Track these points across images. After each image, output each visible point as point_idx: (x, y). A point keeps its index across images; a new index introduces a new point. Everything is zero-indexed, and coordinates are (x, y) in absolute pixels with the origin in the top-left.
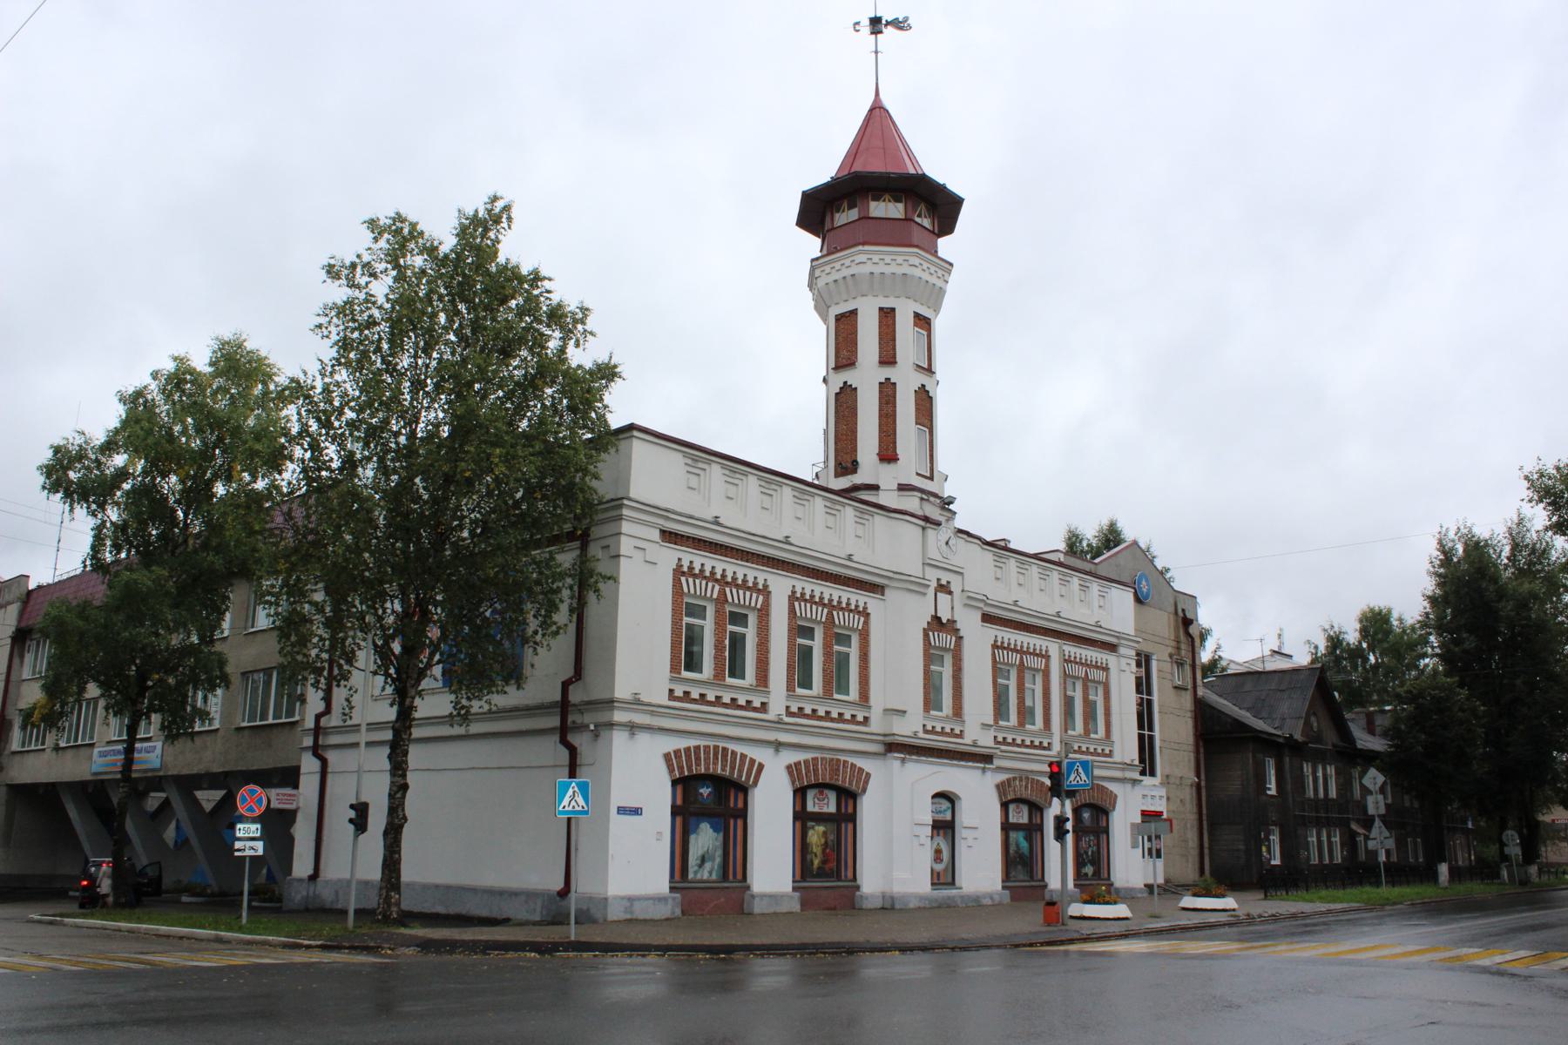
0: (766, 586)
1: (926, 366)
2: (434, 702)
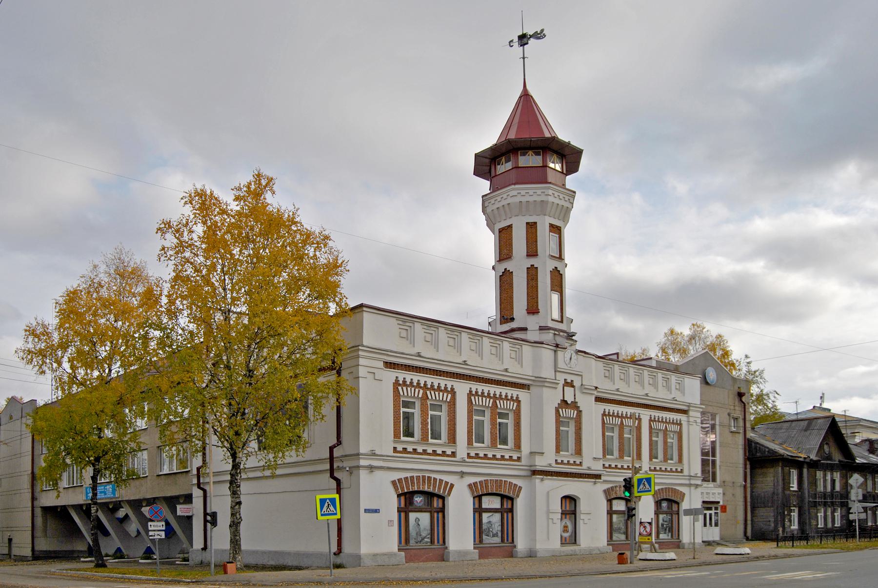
0: (517, 398)
1: (558, 256)
2: (253, 459)
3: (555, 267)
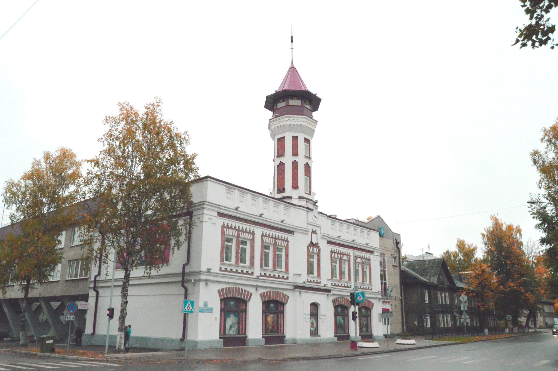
0: (253, 232)
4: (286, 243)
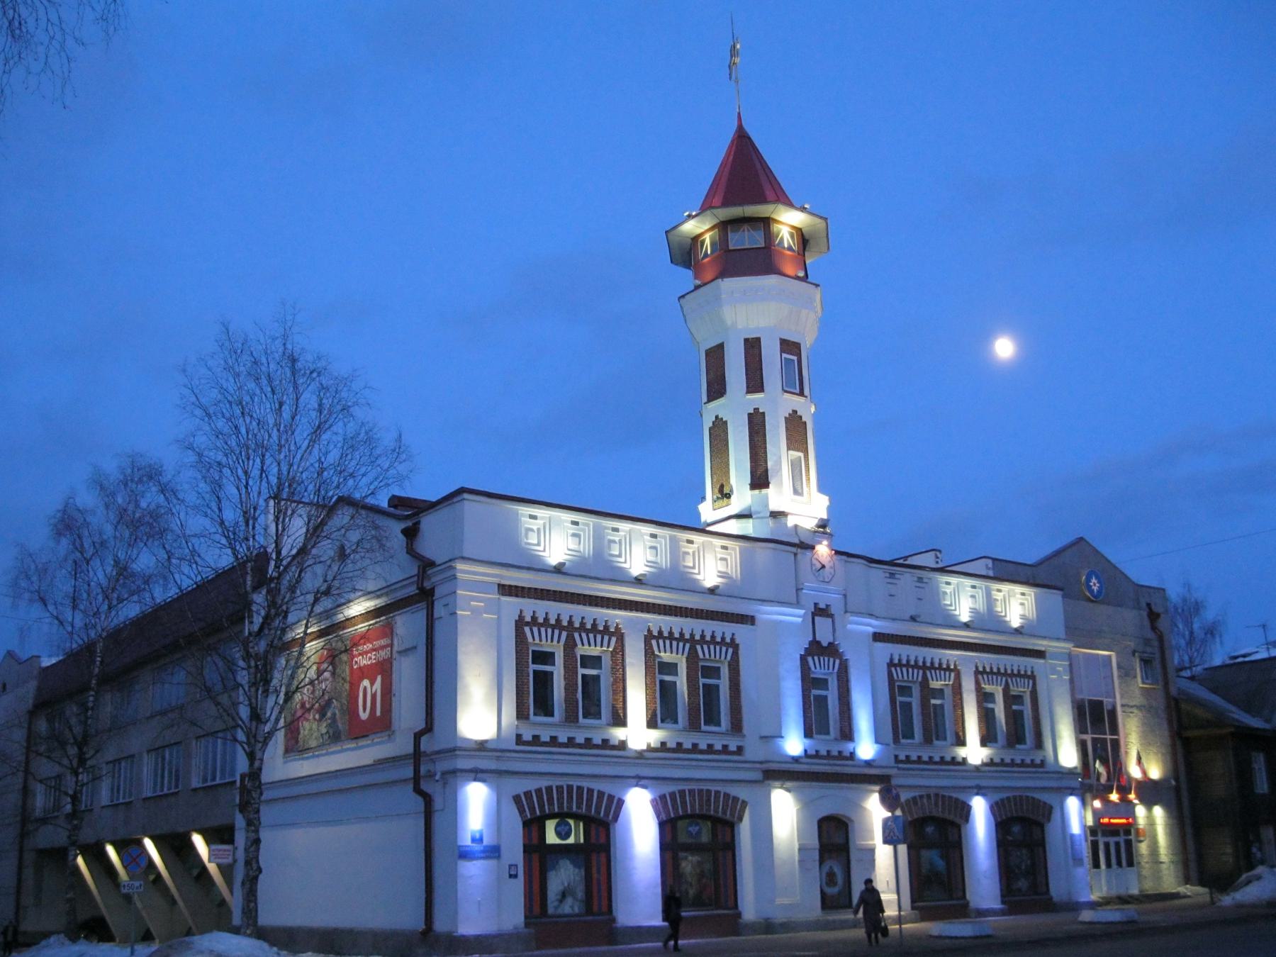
0: (733, 639)
3: (793, 411)
4: (1031, 682)
